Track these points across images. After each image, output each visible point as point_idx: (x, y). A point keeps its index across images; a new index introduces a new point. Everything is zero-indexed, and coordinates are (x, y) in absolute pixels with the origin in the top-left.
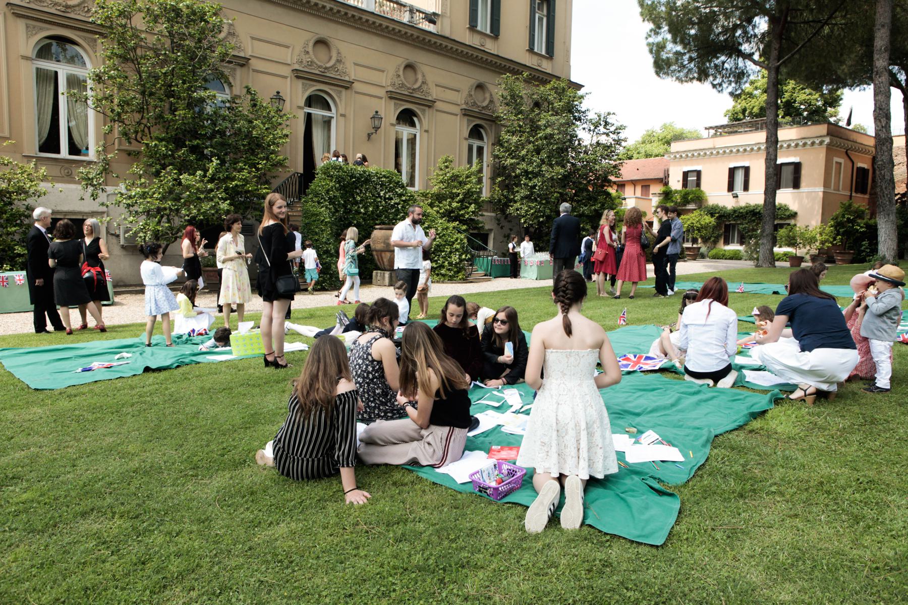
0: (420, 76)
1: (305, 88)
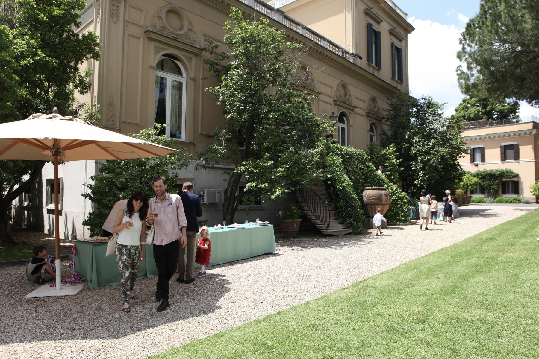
0: (186, 24)
1: (157, 52)
